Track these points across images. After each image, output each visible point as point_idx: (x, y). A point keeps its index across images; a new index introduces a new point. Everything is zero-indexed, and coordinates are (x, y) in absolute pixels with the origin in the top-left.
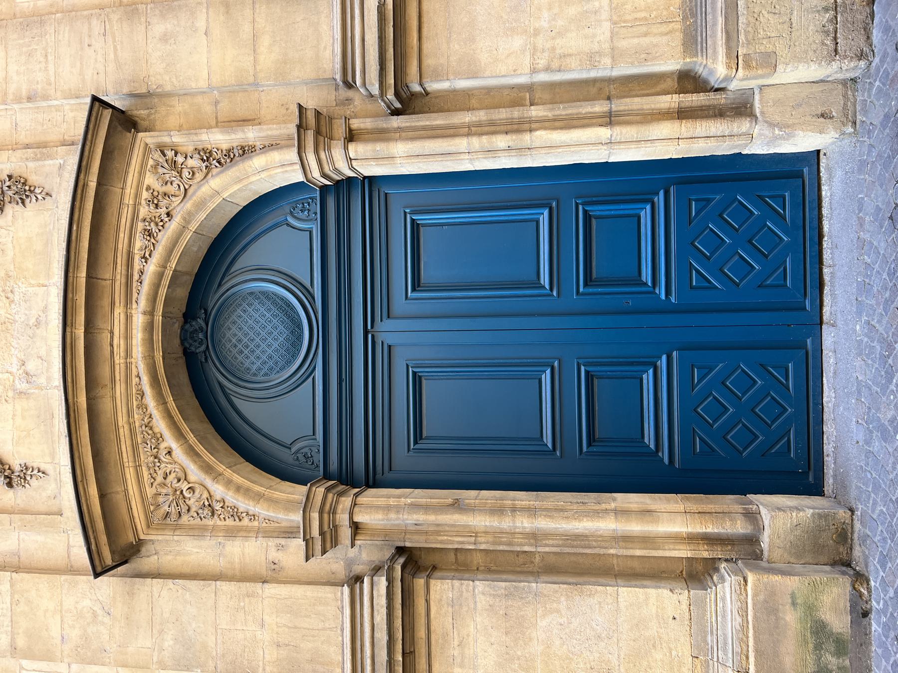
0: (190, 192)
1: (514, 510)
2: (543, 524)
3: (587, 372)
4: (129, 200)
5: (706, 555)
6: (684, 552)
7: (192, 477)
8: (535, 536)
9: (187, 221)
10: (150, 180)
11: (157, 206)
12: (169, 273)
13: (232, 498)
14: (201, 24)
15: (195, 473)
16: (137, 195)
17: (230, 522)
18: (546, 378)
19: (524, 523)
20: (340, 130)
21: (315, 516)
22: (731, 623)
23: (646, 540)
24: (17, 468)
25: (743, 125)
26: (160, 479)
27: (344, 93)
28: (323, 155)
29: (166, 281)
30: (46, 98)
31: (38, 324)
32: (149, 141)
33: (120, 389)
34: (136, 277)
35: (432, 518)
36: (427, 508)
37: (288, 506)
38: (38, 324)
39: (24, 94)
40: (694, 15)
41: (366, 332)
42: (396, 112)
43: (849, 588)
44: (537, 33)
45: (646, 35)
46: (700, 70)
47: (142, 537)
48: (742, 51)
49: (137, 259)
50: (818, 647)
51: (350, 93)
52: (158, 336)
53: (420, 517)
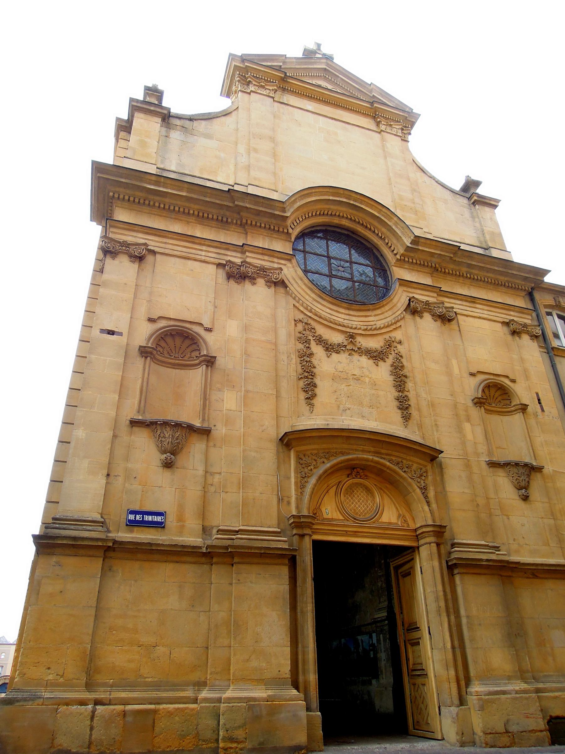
14: (466, 491)
16: (410, 460)
28: (431, 533)
29: (382, 468)
33: (346, 446)
34: (383, 456)
38: (363, 417)
39: (438, 423)
46: (473, 682)
52: (364, 463)
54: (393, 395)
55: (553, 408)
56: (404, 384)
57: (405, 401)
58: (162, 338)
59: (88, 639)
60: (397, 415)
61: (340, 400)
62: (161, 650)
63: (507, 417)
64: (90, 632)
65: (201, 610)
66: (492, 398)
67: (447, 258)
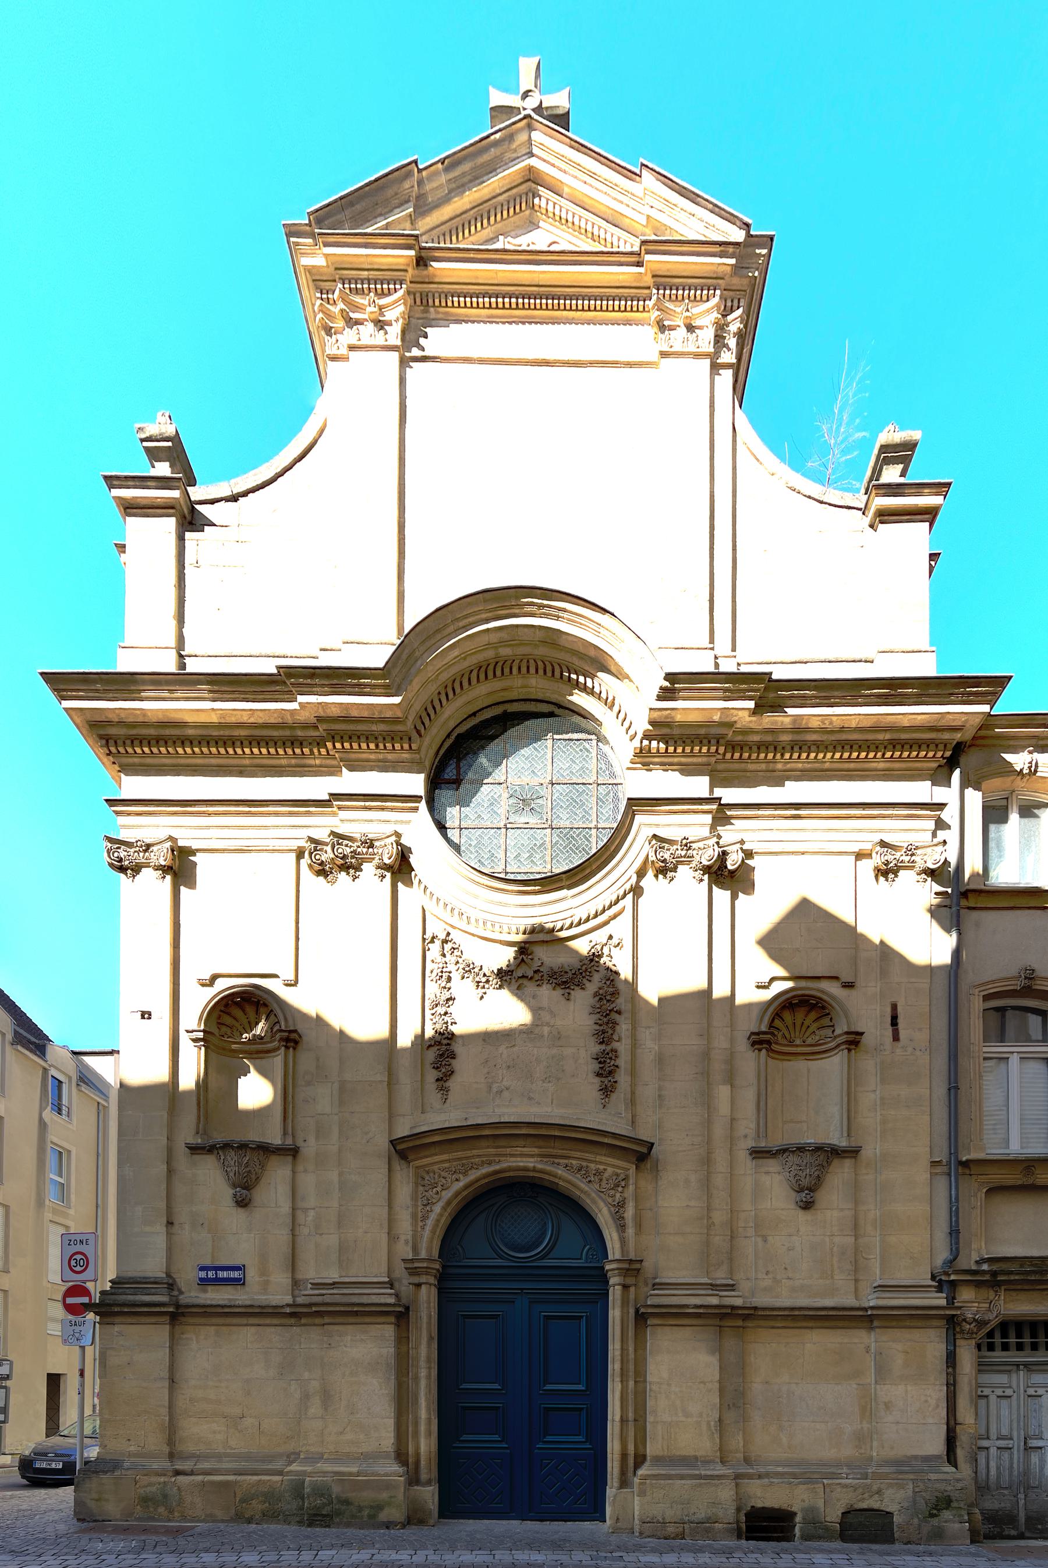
0: (602, 1194)
1: (430, 1368)
2: (423, 1383)
3: (499, 1407)
4: (599, 1158)
5: (410, 1460)
6: (411, 1450)
7: (444, 1193)
8: (416, 1379)
9: (585, 1193)
10: (610, 1170)
11: (595, 1175)
12: (557, 1181)
13: (433, 1216)
14: (693, 1203)
15: (447, 1195)
16: (601, 1163)
17: (420, 1215)
18: (496, 1386)
19: (423, 1373)
20: (630, 1281)
21: (425, 1265)
22: (381, 1470)
23: (416, 1433)
24: (447, 1084)
25: (616, 1484)
26: (443, 1174)
27: (650, 1282)
28: (616, 1272)
30: (660, 1106)
31: (530, 1099)
32: (631, 1171)
33: (492, 1151)
34: (556, 1161)
35: (425, 1326)
36: (429, 1323)
37: (429, 1249)
38: (530, 1099)
40: (670, 1461)
41: (522, 1289)
42: (637, 1311)
43: (399, 1521)
44: (669, 1385)
45: (663, 1438)
47: (411, 1164)
48: (648, 1481)
49: (566, 1161)
50: (371, 1507)
51: (650, 1286)
52: (522, 1174)
53: (425, 1320)
54: (589, 1052)
55: (920, 1029)
56: (613, 1029)
57: (608, 1061)
58: (221, 1011)
59: (164, 1411)
60: (589, 1087)
61: (493, 1074)
62: (248, 1422)
63: (819, 1062)
64: (167, 1404)
65: (293, 1378)
66: (798, 1028)
67: (740, 713)
